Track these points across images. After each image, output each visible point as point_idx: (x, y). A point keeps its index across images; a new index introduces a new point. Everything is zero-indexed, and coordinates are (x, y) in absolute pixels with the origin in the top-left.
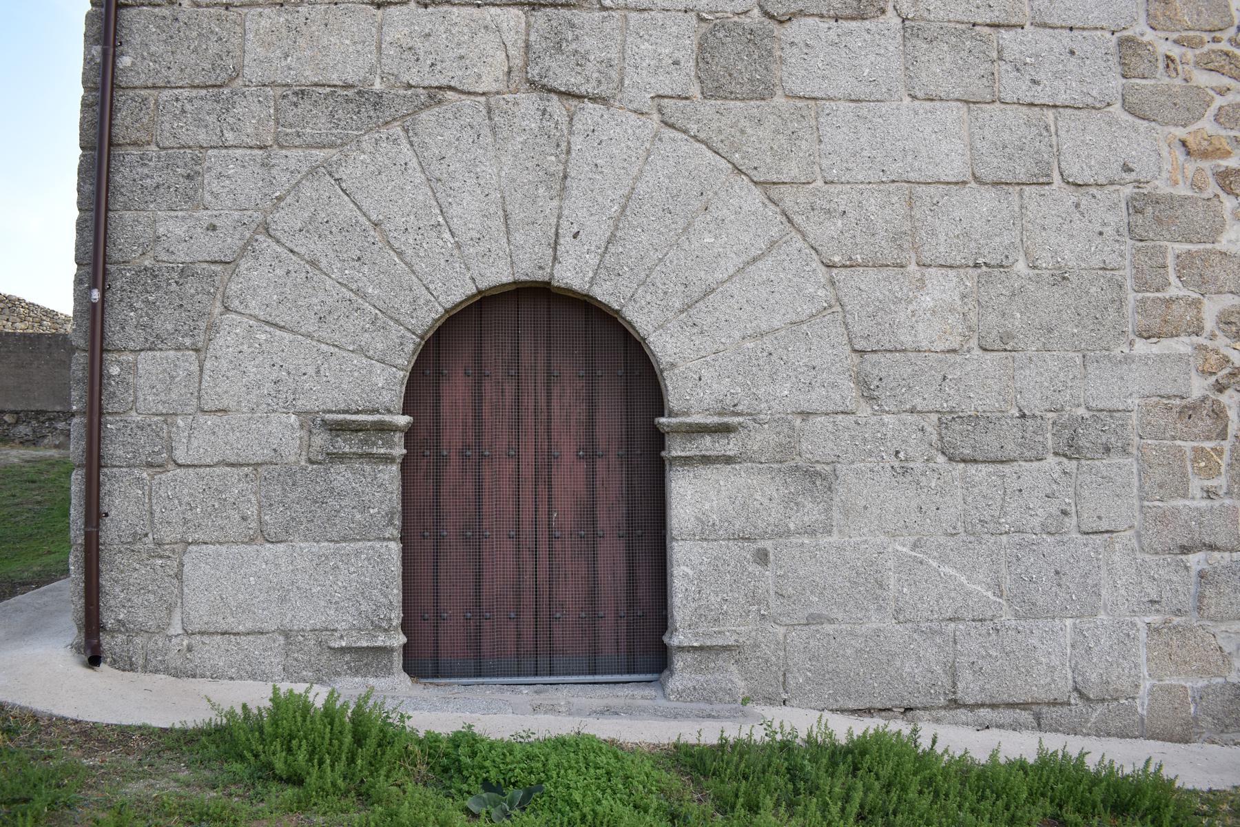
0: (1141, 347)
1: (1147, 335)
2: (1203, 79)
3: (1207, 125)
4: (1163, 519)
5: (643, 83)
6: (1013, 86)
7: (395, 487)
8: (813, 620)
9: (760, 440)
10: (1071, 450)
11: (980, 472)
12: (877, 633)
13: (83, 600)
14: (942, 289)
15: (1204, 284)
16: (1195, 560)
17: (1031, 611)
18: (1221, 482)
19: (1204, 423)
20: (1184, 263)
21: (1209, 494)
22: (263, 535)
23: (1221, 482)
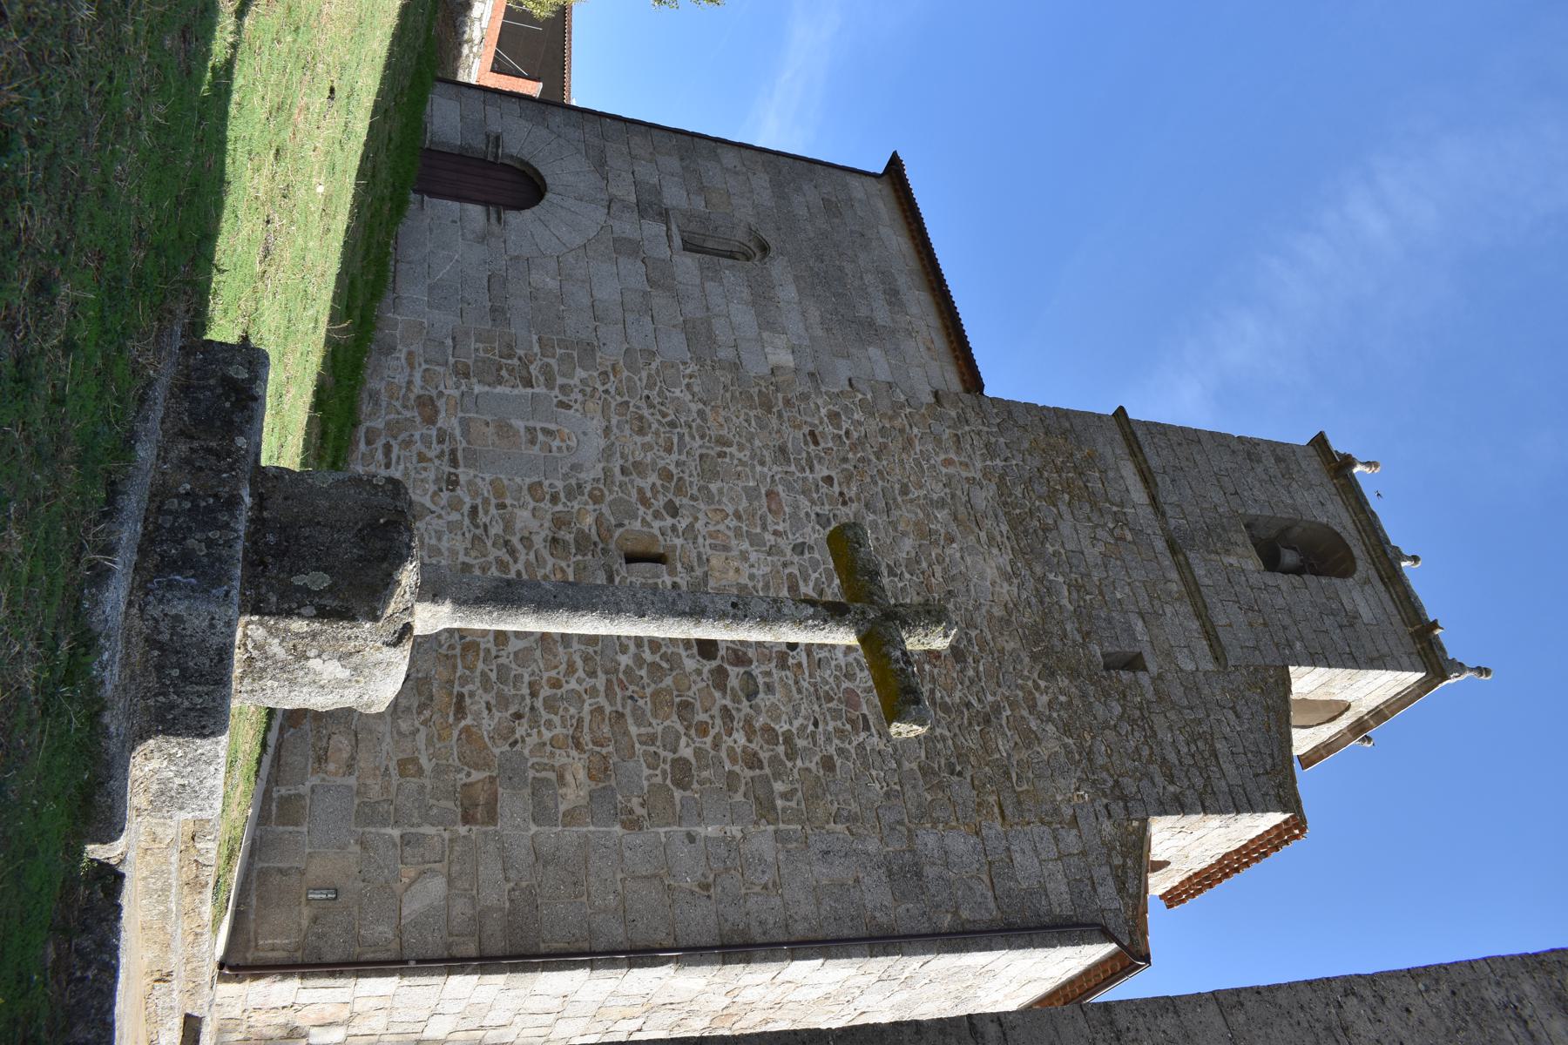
0: (535, 338)
1: (540, 339)
2: (644, 374)
3: (626, 373)
4: (467, 334)
5: (616, 225)
6: (630, 317)
7: (216, 308)
8: (431, 230)
9: (495, 228)
10: (493, 310)
11: (485, 282)
12: (59, 562)
13: (230, 134)
14: (552, 284)
15: (561, 360)
16: (449, 342)
17: (431, 288)
18: (482, 354)
19: (505, 351)
20: (570, 356)
21: (477, 350)
22: (462, 118)
23: (482, 354)
